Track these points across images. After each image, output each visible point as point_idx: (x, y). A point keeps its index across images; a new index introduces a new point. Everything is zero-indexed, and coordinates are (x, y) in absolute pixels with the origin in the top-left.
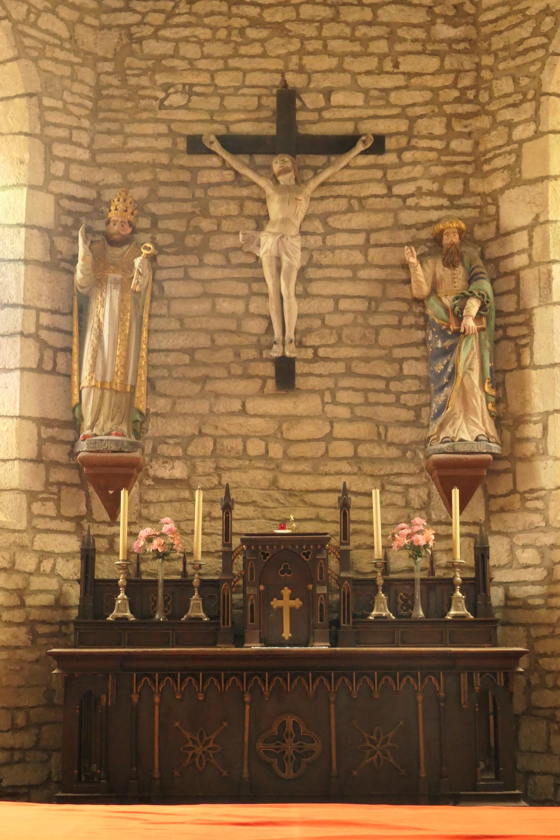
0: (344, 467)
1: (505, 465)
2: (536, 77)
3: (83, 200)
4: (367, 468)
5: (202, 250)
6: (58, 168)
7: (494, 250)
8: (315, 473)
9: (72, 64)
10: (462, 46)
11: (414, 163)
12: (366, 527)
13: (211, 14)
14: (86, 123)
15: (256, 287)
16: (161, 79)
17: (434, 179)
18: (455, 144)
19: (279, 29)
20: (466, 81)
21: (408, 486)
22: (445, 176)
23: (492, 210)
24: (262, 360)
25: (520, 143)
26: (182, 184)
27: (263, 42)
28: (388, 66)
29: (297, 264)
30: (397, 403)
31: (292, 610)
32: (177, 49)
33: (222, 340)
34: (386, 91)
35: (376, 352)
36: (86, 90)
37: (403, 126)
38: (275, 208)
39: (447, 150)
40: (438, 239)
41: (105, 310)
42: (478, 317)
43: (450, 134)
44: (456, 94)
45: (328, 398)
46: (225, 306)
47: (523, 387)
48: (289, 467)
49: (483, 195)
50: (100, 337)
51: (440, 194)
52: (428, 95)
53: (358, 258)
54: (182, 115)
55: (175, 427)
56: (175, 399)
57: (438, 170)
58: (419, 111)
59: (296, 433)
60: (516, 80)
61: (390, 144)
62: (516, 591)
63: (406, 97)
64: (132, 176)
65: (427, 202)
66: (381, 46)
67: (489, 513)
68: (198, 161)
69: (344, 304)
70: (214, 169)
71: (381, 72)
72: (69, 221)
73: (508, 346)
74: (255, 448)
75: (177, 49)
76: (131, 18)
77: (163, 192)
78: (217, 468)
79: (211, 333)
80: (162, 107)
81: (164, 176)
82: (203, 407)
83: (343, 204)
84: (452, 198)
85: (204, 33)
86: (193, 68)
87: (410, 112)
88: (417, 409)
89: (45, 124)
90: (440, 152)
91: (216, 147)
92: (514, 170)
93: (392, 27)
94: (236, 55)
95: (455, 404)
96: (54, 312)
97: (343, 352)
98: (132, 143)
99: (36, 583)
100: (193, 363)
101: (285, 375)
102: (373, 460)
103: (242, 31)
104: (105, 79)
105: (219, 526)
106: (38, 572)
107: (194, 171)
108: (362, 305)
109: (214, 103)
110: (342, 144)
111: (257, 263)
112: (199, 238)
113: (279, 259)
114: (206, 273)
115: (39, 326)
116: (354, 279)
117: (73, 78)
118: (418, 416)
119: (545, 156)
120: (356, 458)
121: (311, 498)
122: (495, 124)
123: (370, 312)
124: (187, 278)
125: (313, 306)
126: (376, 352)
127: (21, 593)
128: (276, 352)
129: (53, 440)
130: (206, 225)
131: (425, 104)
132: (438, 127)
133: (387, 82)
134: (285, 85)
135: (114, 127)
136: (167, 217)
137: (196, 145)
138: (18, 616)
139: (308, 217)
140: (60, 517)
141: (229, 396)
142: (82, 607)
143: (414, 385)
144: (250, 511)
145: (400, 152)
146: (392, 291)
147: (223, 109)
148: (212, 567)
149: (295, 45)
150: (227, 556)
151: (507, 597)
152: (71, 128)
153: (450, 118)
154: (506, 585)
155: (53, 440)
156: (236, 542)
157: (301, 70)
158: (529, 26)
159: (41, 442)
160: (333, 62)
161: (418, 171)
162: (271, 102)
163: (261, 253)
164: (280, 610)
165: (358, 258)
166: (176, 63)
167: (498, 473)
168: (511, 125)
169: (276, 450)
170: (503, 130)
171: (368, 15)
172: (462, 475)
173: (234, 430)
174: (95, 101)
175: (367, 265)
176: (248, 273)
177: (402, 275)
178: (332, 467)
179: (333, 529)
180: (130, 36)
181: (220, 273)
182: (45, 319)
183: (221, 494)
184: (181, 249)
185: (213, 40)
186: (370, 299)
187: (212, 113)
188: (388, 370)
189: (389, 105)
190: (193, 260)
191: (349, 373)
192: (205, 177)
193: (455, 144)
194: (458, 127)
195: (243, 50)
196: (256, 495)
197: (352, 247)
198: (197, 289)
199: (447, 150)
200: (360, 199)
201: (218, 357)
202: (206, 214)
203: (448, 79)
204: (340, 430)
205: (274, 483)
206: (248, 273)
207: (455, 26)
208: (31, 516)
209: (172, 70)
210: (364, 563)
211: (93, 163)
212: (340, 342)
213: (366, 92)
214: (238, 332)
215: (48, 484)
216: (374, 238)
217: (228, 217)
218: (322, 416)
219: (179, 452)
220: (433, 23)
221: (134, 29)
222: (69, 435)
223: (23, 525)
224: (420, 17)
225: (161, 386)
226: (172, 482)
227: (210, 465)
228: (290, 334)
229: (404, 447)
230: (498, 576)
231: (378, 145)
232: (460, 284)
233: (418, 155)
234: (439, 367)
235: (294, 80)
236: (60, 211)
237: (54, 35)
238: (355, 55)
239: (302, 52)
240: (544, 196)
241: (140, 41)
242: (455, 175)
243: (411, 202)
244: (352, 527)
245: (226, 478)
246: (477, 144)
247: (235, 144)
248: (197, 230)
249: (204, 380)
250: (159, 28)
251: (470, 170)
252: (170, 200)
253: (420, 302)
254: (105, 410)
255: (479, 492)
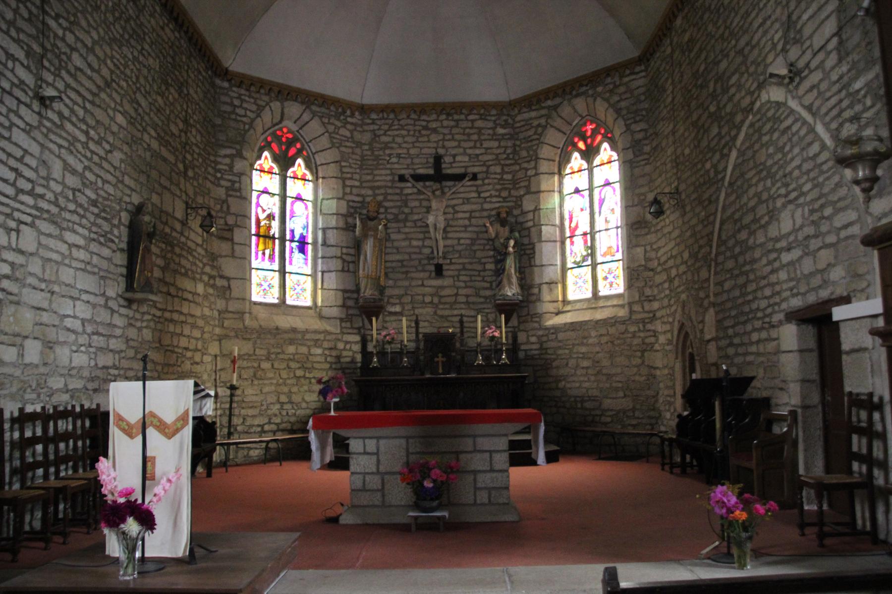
0: (463, 306)
1: (525, 304)
2: (536, 151)
3: (358, 202)
4: (471, 306)
5: (406, 220)
6: (348, 190)
7: (521, 219)
8: (451, 308)
9: (352, 148)
10: (507, 137)
11: (489, 184)
12: (473, 330)
13: (407, 125)
14: (358, 171)
15: (427, 235)
16: (388, 152)
17: (497, 190)
18: (505, 176)
19: (435, 130)
20: (509, 151)
21: (487, 313)
22: (501, 189)
23: (519, 203)
24: (430, 264)
25: (530, 177)
26: (397, 194)
27: (428, 136)
28: (478, 145)
29: (442, 226)
30: (483, 281)
31: (443, 362)
32: (394, 140)
33: (414, 256)
34: (477, 155)
35: (475, 260)
36: (358, 157)
37: (484, 169)
38: (434, 204)
39: (502, 179)
40: (498, 214)
41: (369, 247)
42: (514, 247)
43: (503, 172)
44: (505, 156)
45: (456, 279)
46: (415, 243)
47: (532, 274)
48: (441, 306)
49: (516, 197)
50: (366, 255)
51: (499, 196)
52: (494, 157)
53: (467, 222)
54: (396, 166)
55: (396, 292)
56: (395, 280)
57: (498, 187)
58: (490, 163)
59: (443, 293)
60: (528, 152)
61: (479, 176)
62: (529, 353)
63: (486, 158)
64: (377, 192)
65: (494, 200)
66: (475, 137)
67: (519, 323)
68: (402, 185)
69: (462, 241)
70: (409, 188)
71: (475, 147)
72: (352, 211)
73: (526, 257)
74: (428, 299)
75: (394, 140)
76: (376, 127)
77: (389, 197)
78: (413, 308)
79: (409, 254)
80: (388, 163)
81: (390, 191)
82: (406, 283)
83: (461, 201)
84: (504, 198)
85: (404, 132)
86: (400, 147)
87: (487, 163)
88: (491, 283)
89: (342, 173)
90: (499, 180)
91: (410, 179)
92: (528, 187)
93: (480, 129)
94: (417, 141)
95: (505, 281)
96: (347, 247)
97: (461, 261)
98: (377, 178)
99: (345, 353)
100: (403, 266)
101: (439, 271)
102: (473, 303)
103: (420, 131)
104: (365, 153)
105: (414, 330)
106: (345, 349)
107: (402, 189)
108: (468, 242)
109: (409, 161)
110: (459, 178)
111: (427, 226)
112: (404, 216)
113: (435, 225)
114: (407, 230)
115: (342, 254)
116: (465, 231)
117: (353, 153)
118: (491, 285)
119: (539, 184)
120: (467, 303)
121: (450, 319)
122: (521, 169)
123: (472, 244)
124: (399, 232)
125: (449, 242)
126: (475, 260)
127: (338, 357)
128: (435, 261)
129: (349, 298)
130: (406, 210)
131: (493, 160)
132: (498, 169)
133: (478, 152)
134: (437, 153)
135: (369, 171)
136: (392, 208)
137: (402, 178)
138: (338, 366)
139: (447, 207)
140: (352, 328)
141: (417, 279)
142: (362, 362)
143: (490, 273)
144: (426, 324)
145: (483, 180)
146: (481, 236)
147: (413, 163)
148: (412, 346)
149: (441, 137)
150: (417, 340)
151: (526, 355)
152: (352, 173)
153: (503, 166)
154: (526, 350)
155: (349, 298)
156: (421, 336)
157: (444, 147)
158: (533, 130)
159: (344, 299)
160: (456, 144)
161: (490, 187)
162: (431, 160)
163: (429, 222)
164: (438, 362)
165: (467, 222)
166: (394, 145)
167: (523, 307)
168: (527, 170)
169: (436, 300)
170: (524, 171)
171: (470, 125)
172: (508, 309)
173: (420, 292)
174: (361, 161)
175: (470, 225)
176: (424, 229)
177: (484, 229)
178: (458, 306)
179: (458, 330)
180: (375, 135)
181: (412, 230)
182: (344, 250)
183: (414, 318)
184: (396, 220)
185: (408, 135)
186: (472, 239)
187: (408, 165)
188: (480, 267)
189: (479, 161)
190: (402, 225)
191: (464, 269)
192: (406, 191)
193: (505, 176)
194: (506, 169)
195: (420, 139)
196: (428, 318)
197: (465, 218)
198: (403, 236)
199: (502, 179)
200: (468, 199)
201: (412, 263)
202: (406, 206)
203: (502, 150)
204: (461, 292)
205: (435, 313)
206: (424, 229)
207: (505, 128)
208: (342, 328)
209: (392, 148)
210: (472, 343)
211: (361, 187)
212: (460, 257)
213: (470, 155)
214: (420, 253)
215: (347, 315)
216: (473, 214)
217: (415, 207)
218: (454, 286)
219: (398, 301)
220: (496, 128)
221: (377, 132)
222: (355, 296)
223: (339, 331)
224: (491, 125)
225: (391, 275)
226: (395, 314)
227: (410, 307)
228: (440, 254)
229: (486, 297)
230: (523, 347)
231: (474, 177)
232: (507, 234)
233: (490, 181)
234: (499, 266)
235: (441, 151)
236: (349, 207)
237: (345, 137)
238: (465, 141)
239: (444, 140)
240: (539, 198)
241: (379, 136)
242: (506, 189)
243: (488, 200)
244: (465, 330)
245: (417, 311)
246: (514, 176)
247: (418, 178)
248: (403, 213)
249: (407, 272)
250: (386, 131)
251: (511, 186)
252: (392, 201)
253: (493, 240)
254: (369, 286)
255: (515, 315)
